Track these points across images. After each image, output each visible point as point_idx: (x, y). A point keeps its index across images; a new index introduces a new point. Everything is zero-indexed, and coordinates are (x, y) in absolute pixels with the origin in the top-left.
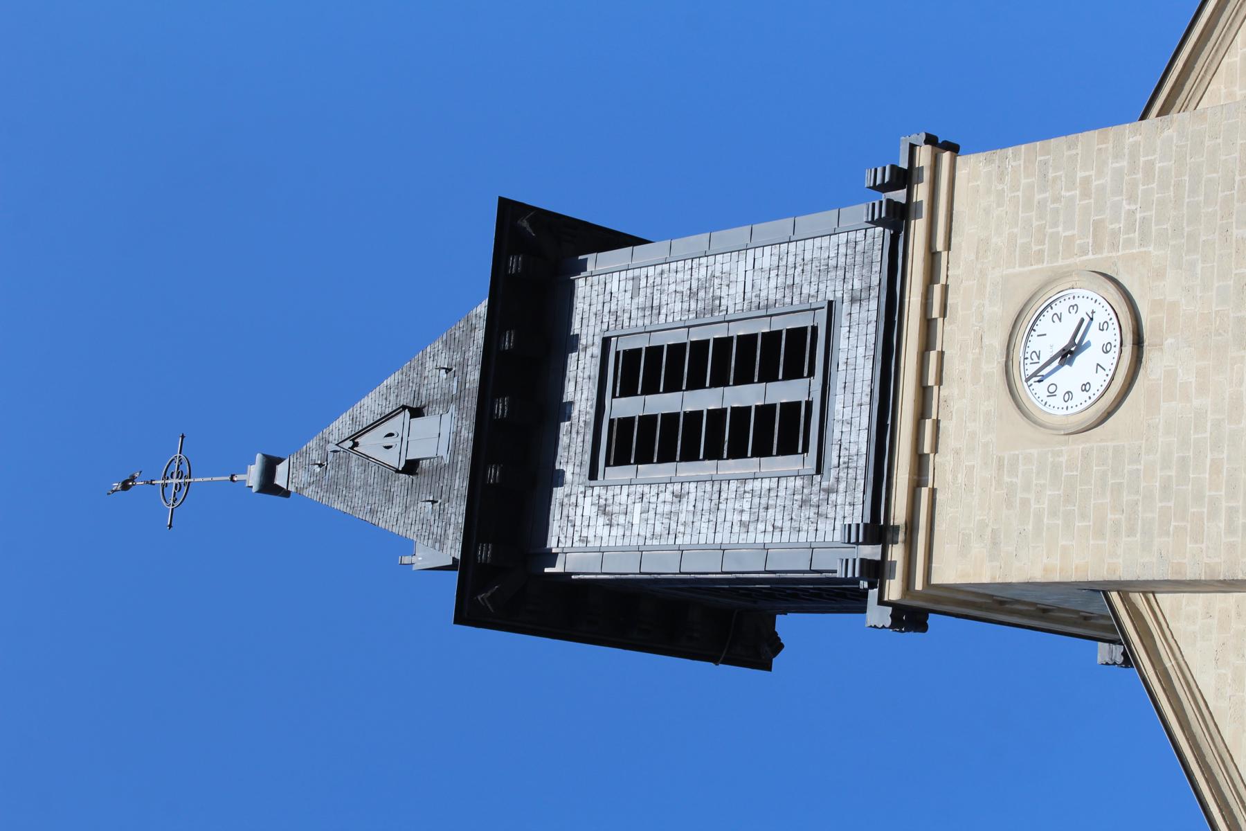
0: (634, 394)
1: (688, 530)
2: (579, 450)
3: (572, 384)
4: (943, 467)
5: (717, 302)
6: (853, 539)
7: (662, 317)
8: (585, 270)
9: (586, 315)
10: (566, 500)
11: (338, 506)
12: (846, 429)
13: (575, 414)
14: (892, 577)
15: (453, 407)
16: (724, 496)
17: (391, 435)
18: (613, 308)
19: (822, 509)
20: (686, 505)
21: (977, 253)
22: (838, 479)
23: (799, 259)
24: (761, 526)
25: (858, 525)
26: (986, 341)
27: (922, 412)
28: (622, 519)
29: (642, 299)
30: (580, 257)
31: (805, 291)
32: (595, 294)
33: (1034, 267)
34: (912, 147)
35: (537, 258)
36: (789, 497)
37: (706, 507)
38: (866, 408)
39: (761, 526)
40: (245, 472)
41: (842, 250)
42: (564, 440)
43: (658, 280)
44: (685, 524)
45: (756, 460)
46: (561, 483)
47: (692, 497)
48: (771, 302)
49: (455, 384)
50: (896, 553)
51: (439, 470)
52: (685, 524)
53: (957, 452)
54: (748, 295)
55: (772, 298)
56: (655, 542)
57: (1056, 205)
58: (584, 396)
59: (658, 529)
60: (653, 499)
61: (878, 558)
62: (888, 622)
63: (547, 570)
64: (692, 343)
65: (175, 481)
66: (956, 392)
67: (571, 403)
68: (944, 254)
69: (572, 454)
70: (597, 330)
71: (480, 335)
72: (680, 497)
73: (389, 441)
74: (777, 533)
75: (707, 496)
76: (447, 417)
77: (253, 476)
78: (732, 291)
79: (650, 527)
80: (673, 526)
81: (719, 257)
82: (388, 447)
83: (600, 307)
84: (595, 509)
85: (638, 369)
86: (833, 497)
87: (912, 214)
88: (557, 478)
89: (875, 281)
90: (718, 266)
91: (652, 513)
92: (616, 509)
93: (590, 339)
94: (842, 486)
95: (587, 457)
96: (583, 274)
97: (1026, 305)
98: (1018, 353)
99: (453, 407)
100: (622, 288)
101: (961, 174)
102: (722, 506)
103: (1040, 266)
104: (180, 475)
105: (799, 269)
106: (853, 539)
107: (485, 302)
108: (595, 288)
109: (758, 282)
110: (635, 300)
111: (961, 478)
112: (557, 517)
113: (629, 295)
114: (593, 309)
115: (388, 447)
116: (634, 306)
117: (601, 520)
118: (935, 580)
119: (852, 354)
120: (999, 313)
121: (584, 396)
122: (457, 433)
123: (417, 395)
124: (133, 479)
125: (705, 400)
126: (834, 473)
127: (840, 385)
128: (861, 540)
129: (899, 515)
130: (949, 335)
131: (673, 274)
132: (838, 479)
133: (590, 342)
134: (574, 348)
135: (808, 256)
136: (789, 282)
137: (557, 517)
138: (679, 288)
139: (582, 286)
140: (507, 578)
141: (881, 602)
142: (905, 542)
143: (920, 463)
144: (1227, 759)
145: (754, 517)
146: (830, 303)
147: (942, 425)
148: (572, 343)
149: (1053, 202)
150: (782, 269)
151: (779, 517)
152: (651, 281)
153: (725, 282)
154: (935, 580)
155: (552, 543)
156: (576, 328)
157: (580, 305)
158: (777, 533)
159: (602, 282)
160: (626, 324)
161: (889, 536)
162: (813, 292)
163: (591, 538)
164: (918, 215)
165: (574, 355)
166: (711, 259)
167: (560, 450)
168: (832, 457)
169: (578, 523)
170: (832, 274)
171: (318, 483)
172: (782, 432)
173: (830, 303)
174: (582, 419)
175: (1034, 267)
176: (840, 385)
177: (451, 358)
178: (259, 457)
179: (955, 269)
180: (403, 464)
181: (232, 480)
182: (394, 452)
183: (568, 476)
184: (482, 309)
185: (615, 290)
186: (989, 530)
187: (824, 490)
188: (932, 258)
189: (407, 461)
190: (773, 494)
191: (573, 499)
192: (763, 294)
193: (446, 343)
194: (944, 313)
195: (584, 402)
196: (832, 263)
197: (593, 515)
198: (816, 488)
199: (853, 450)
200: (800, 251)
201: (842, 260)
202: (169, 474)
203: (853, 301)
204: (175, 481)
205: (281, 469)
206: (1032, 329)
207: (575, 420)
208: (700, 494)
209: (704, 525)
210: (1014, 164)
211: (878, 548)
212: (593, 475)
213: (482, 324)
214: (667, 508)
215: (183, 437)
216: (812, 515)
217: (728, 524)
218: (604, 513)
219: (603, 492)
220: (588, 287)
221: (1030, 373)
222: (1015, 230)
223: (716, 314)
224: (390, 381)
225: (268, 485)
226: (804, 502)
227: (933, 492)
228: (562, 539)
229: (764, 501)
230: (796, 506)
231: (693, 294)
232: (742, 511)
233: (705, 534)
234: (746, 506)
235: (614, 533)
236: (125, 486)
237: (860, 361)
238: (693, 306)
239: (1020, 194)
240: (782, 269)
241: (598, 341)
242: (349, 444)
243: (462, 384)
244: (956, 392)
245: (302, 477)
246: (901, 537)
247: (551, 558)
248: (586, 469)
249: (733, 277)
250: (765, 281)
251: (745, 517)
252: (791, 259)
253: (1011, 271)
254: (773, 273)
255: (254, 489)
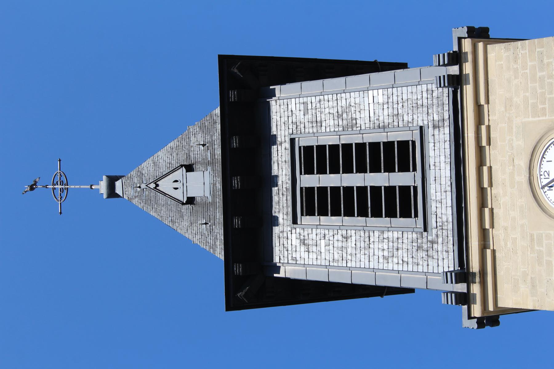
0: (313, 173)
1: (354, 259)
2: (285, 205)
3: (276, 165)
4: (498, 237)
5: (354, 121)
6: (441, 63)
7: (323, 128)
8: (275, 96)
9: (279, 124)
10: (281, 235)
11: (152, 213)
12: (439, 205)
13: (280, 183)
14: (475, 303)
15: (209, 168)
16: (372, 240)
17: (176, 181)
18: (294, 120)
19: (430, 253)
20: (351, 243)
21: (506, 107)
22: (437, 236)
23: (400, 99)
24: (395, 260)
25: (444, 76)
26: (516, 162)
28: (314, 248)
29: (310, 116)
30: (271, 87)
31: (406, 118)
32: (282, 111)
33: (541, 118)
34: (460, 39)
35: (247, 87)
36: (410, 244)
37: (362, 245)
38: (449, 194)
39: (395, 260)
40: (98, 185)
41: (425, 95)
42: (275, 199)
43: (318, 105)
44: (351, 255)
45: (388, 219)
46: (277, 225)
47: (353, 238)
48: (386, 124)
49: (209, 154)
50: (476, 289)
51: (206, 205)
52: (351, 255)
53: (506, 229)
54: (372, 119)
55: (386, 121)
56: (336, 264)
57: (550, 80)
58: (284, 173)
59: (336, 257)
60: (331, 238)
61: (457, 73)
62: (476, 326)
63: (275, 275)
64: (342, 144)
65: (59, 187)
66: (501, 192)
67: (277, 176)
68: (486, 106)
69: (281, 207)
70: (287, 133)
71: (219, 126)
72: (347, 238)
73: (176, 185)
74: (405, 265)
75: (362, 239)
76: (207, 173)
77: (102, 187)
78: (362, 116)
79: (331, 255)
80: (345, 255)
81: (352, 94)
82: (176, 189)
83: (286, 119)
84: (298, 241)
85: (314, 158)
86: (435, 246)
87: (464, 82)
88: (274, 221)
89: (446, 117)
90: (353, 100)
91: (331, 247)
92: (310, 242)
93: (283, 138)
94: (440, 240)
95: (290, 209)
96: (274, 98)
97: (538, 143)
98: (536, 172)
99: (209, 168)
100: (298, 109)
101: (490, 56)
102: (371, 246)
103: (544, 118)
104: (62, 183)
105: (400, 105)
106: (441, 63)
107: (219, 108)
108: (282, 107)
109: (377, 111)
110: (306, 117)
111: (509, 245)
112: (277, 244)
113: (302, 113)
114: (283, 120)
115: (176, 189)
116: (306, 121)
117: (303, 248)
118: (500, 305)
119: (437, 160)
120: (522, 146)
121: (284, 173)
122: (214, 185)
123: (188, 156)
124: (35, 184)
125: (354, 180)
126: (434, 231)
127: (432, 178)
128: (446, 62)
129: (475, 266)
130: (493, 156)
131: (326, 103)
132: (437, 236)
133: (283, 140)
134: (275, 143)
135: (405, 98)
136: (396, 112)
137: (277, 244)
138: (331, 111)
140: (252, 280)
141: (470, 317)
142: (480, 282)
143: (484, 234)
145: (391, 254)
146: (421, 128)
147: (495, 211)
148: (272, 140)
149: (548, 78)
150: (390, 104)
151: (405, 255)
152: (314, 105)
153: (358, 110)
154: (500, 305)
155: (276, 260)
156: (274, 131)
157: (275, 117)
158: (405, 265)
159: (285, 103)
160: (303, 131)
161: (470, 279)
162: (410, 120)
163: (298, 259)
164: (467, 83)
165: (275, 147)
166: (348, 94)
167: (274, 204)
168: (432, 222)
169: (290, 249)
170: (420, 109)
171: (140, 197)
172: (401, 204)
173: (421, 128)
174: (284, 186)
175: (541, 118)
176: (432, 178)
177: (204, 136)
178: (104, 177)
179: (495, 115)
180: (185, 200)
181: (91, 188)
182: (180, 191)
183: (281, 220)
184: (218, 111)
185: (294, 109)
186: (529, 277)
187: (430, 242)
188: (479, 109)
189: (188, 198)
190: (400, 241)
191: (285, 235)
192: (381, 119)
193: (200, 128)
194: (489, 143)
195: (284, 176)
196: (420, 102)
197: (298, 245)
198: (425, 240)
199: (444, 219)
200: (400, 94)
201: (425, 101)
202: (55, 182)
203: (434, 127)
204: (59, 187)
205: (118, 184)
206: (543, 157)
207: (281, 187)
208: (358, 237)
209: (363, 257)
210: (523, 52)
211: (465, 285)
212: (295, 221)
213: (219, 120)
214: (340, 244)
215: (60, 160)
216: (424, 255)
217: (376, 257)
218: (304, 244)
219: (302, 231)
220: (278, 106)
221: (543, 184)
222: (527, 94)
223: (355, 129)
224: (172, 144)
225: (112, 193)
226: (419, 248)
227: (494, 252)
228: (282, 258)
229: (395, 245)
230: (414, 250)
231: (340, 116)
232: (383, 250)
233: (364, 263)
234: (386, 247)
235: (311, 256)
236: (32, 188)
237: (443, 165)
238: (341, 123)
239: (528, 71)
240: (390, 104)
241: (288, 140)
242: (153, 186)
243: (213, 155)
244: (501, 192)
245: (130, 192)
246: (478, 279)
247: (277, 269)
248: (290, 217)
249: (362, 107)
250: (381, 111)
251: (386, 253)
252: (395, 98)
253: (526, 120)
254: (386, 106)
255: (105, 196)
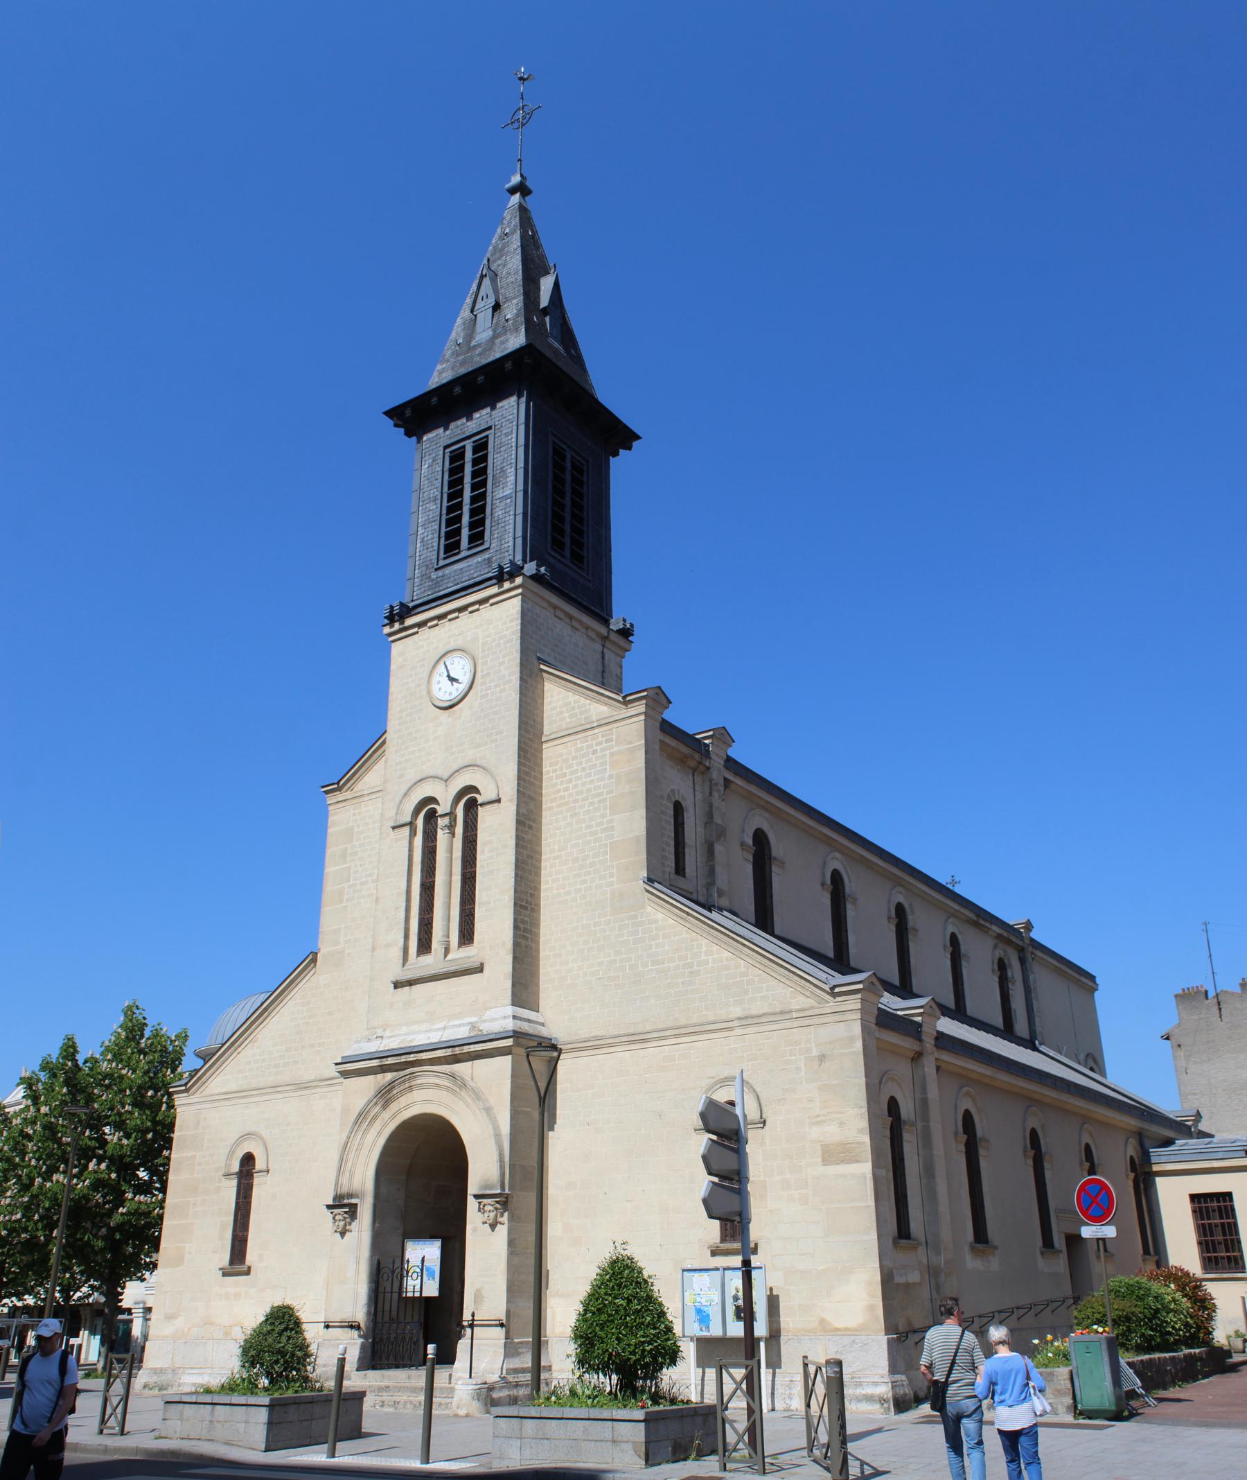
4: (424, 632)
27: (440, 617)
42: (459, 422)
50: (397, 626)
130: (446, 627)
139: (513, 400)
144: (368, 770)
148: (470, 418)
156: (499, 405)
179: (486, 611)
183: (448, 432)
